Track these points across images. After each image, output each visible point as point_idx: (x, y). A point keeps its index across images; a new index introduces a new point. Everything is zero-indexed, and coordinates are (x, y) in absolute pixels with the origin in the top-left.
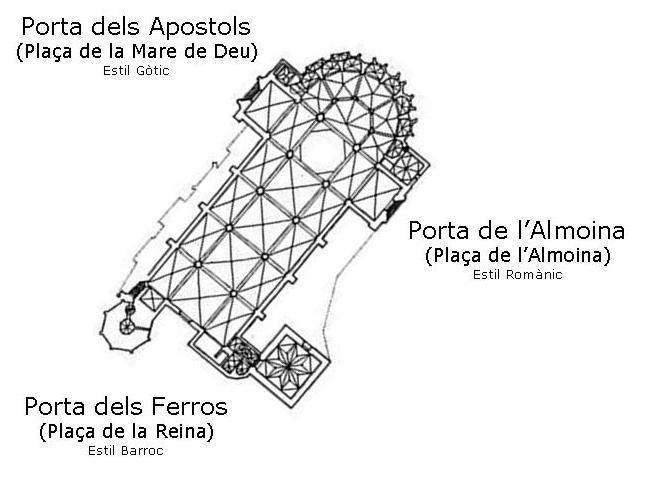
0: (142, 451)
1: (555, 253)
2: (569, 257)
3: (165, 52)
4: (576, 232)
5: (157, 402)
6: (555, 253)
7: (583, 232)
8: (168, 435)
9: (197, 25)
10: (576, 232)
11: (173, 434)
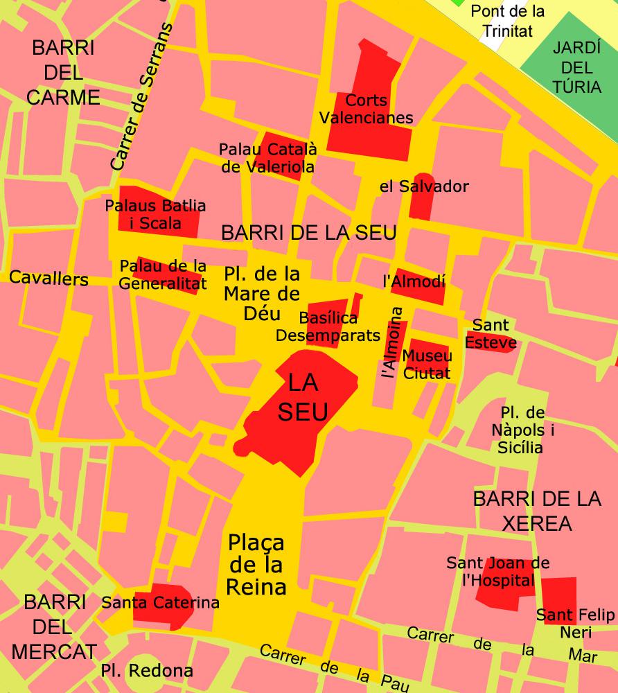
0: (285, 656)
1: (414, 280)
2: (527, 431)
3: (257, 295)
4: (364, 119)
5: (582, 612)
6: (414, 280)
7: (369, 119)
8: (240, 591)
9: (499, 584)
10: (364, 119)
11: (145, 673)
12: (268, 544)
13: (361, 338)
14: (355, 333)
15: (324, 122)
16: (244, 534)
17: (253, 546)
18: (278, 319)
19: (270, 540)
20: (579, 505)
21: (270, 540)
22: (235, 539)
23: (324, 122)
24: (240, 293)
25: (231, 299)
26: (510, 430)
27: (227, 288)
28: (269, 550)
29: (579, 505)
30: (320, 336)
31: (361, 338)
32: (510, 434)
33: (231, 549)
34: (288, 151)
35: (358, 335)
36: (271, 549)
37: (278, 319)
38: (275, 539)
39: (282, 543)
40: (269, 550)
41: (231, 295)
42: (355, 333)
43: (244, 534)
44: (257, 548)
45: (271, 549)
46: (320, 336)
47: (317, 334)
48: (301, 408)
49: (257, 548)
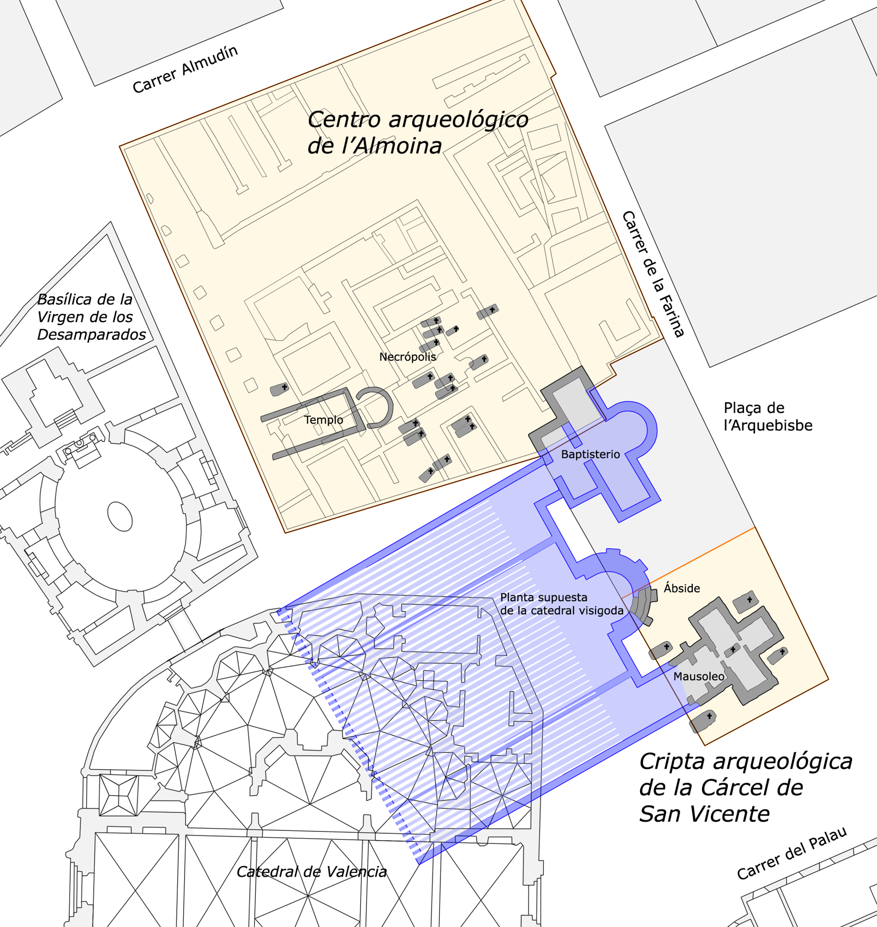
12: (750, 409)
13: (569, 612)
14: (565, 609)
15: (582, 613)
16: (734, 403)
17: (741, 410)
18: (845, 834)
19: (752, 406)
20: (705, 745)
21: (752, 406)
22: (728, 406)
23: (582, 613)
24: (683, 676)
25: (678, 679)
26: (574, 455)
27: (675, 673)
28: (751, 412)
29: (705, 745)
30: (320, 420)
31: (569, 612)
32: (574, 457)
33: (726, 412)
34: (543, 612)
35: (566, 610)
36: (752, 412)
37: (845, 834)
38: (755, 406)
39: (760, 408)
40: (751, 412)
41: (678, 677)
42: (565, 609)
43: (734, 403)
44: (743, 412)
45: (752, 412)
46: (320, 420)
47: (318, 419)
48: (668, 299)
49: (743, 412)
